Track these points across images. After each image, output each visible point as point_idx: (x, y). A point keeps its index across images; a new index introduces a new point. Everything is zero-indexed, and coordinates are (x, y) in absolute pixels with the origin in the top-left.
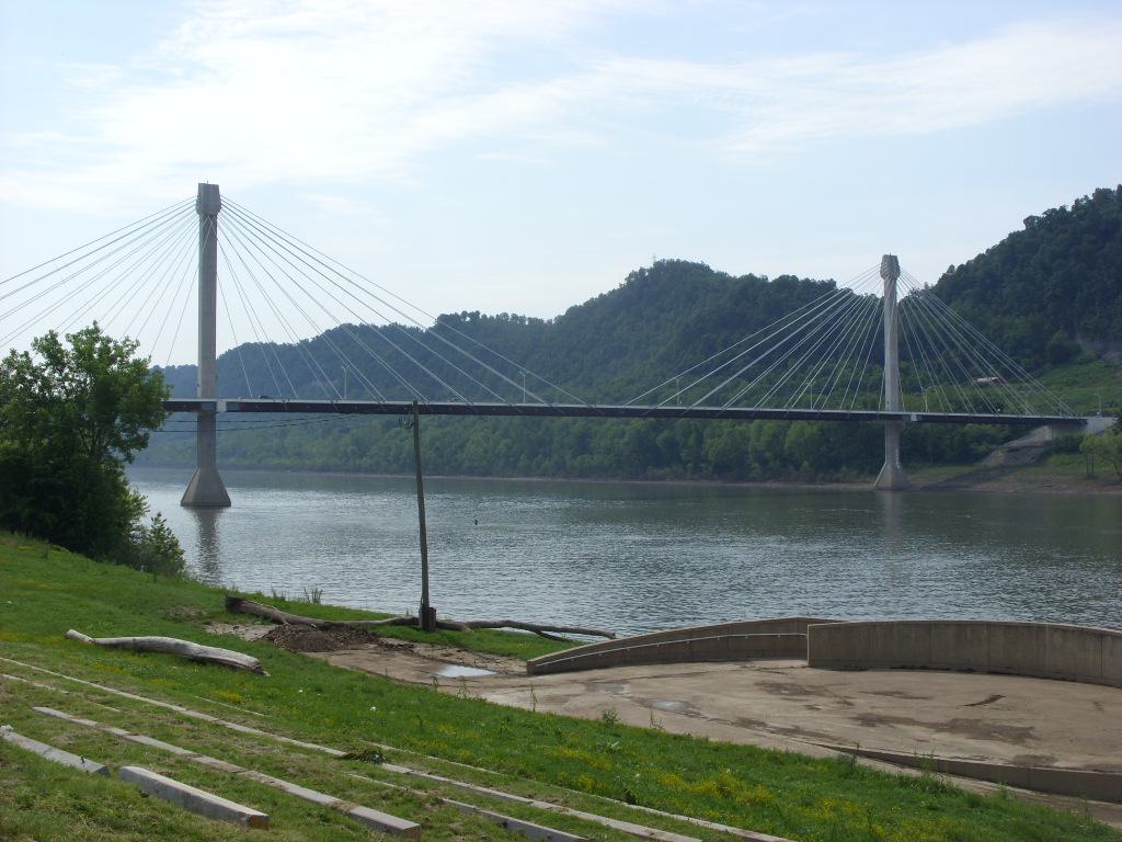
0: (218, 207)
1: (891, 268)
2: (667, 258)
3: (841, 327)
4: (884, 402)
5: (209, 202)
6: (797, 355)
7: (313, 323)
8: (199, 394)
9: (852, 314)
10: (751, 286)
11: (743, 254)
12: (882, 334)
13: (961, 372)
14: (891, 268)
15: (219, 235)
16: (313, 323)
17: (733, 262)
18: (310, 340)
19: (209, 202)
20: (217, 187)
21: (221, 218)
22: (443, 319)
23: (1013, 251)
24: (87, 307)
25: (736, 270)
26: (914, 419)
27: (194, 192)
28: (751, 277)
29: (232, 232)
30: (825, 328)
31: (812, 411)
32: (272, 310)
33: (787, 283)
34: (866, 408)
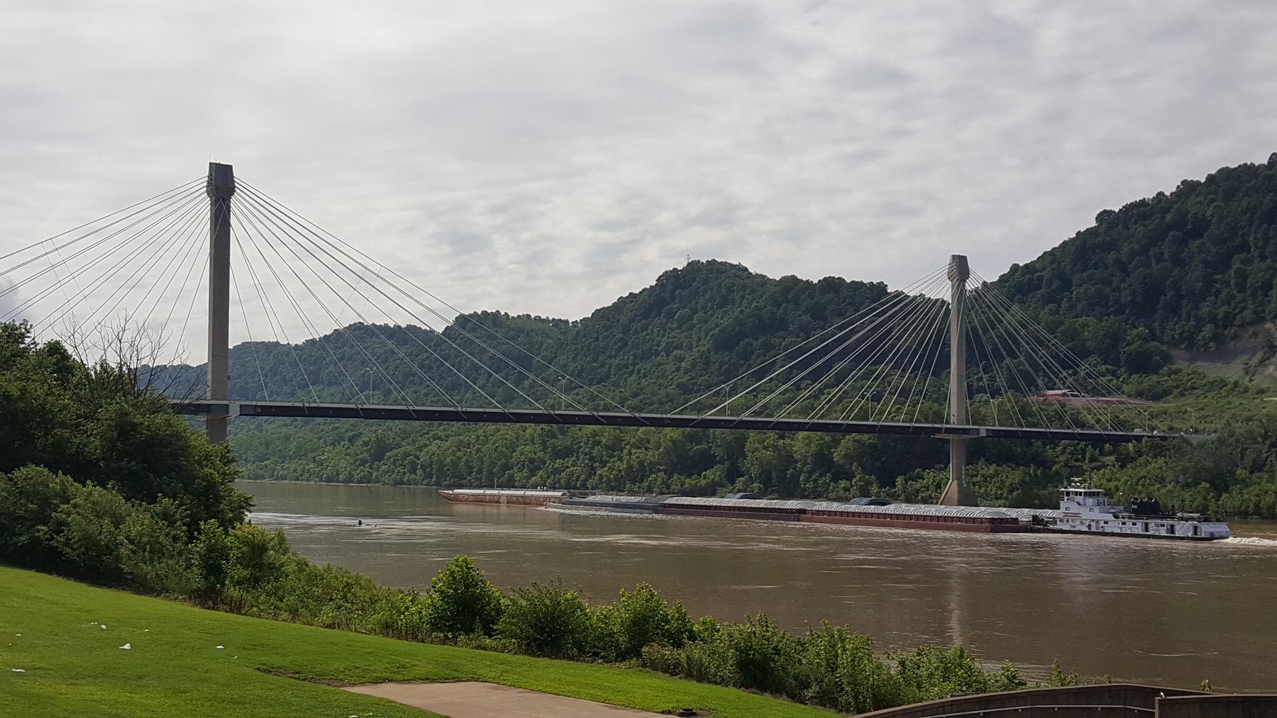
0: (232, 191)
1: (960, 268)
2: (152, 599)
3: (892, 328)
4: (949, 415)
5: (221, 183)
6: (842, 355)
7: (336, 321)
8: (209, 395)
9: (904, 318)
10: (857, 285)
11: (775, 252)
12: (947, 345)
13: (1025, 382)
14: (960, 268)
15: (233, 220)
16: (336, 321)
17: (768, 260)
18: (1168, 194)
19: (221, 183)
20: (229, 168)
21: (235, 202)
22: (462, 320)
23: (1081, 250)
24: (80, 297)
25: (776, 273)
26: (983, 434)
27: (203, 174)
28: (794, 278)
29: (250, 222)
30: (874, 330)
31: (870, 423)
32: (283, 307)
33: (832, 284)
34: (927, 421)
